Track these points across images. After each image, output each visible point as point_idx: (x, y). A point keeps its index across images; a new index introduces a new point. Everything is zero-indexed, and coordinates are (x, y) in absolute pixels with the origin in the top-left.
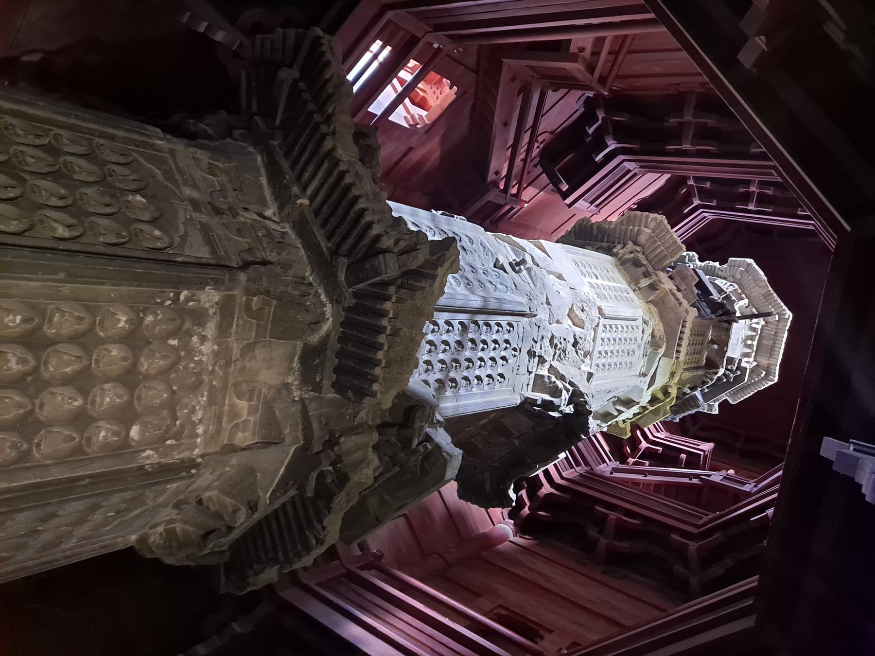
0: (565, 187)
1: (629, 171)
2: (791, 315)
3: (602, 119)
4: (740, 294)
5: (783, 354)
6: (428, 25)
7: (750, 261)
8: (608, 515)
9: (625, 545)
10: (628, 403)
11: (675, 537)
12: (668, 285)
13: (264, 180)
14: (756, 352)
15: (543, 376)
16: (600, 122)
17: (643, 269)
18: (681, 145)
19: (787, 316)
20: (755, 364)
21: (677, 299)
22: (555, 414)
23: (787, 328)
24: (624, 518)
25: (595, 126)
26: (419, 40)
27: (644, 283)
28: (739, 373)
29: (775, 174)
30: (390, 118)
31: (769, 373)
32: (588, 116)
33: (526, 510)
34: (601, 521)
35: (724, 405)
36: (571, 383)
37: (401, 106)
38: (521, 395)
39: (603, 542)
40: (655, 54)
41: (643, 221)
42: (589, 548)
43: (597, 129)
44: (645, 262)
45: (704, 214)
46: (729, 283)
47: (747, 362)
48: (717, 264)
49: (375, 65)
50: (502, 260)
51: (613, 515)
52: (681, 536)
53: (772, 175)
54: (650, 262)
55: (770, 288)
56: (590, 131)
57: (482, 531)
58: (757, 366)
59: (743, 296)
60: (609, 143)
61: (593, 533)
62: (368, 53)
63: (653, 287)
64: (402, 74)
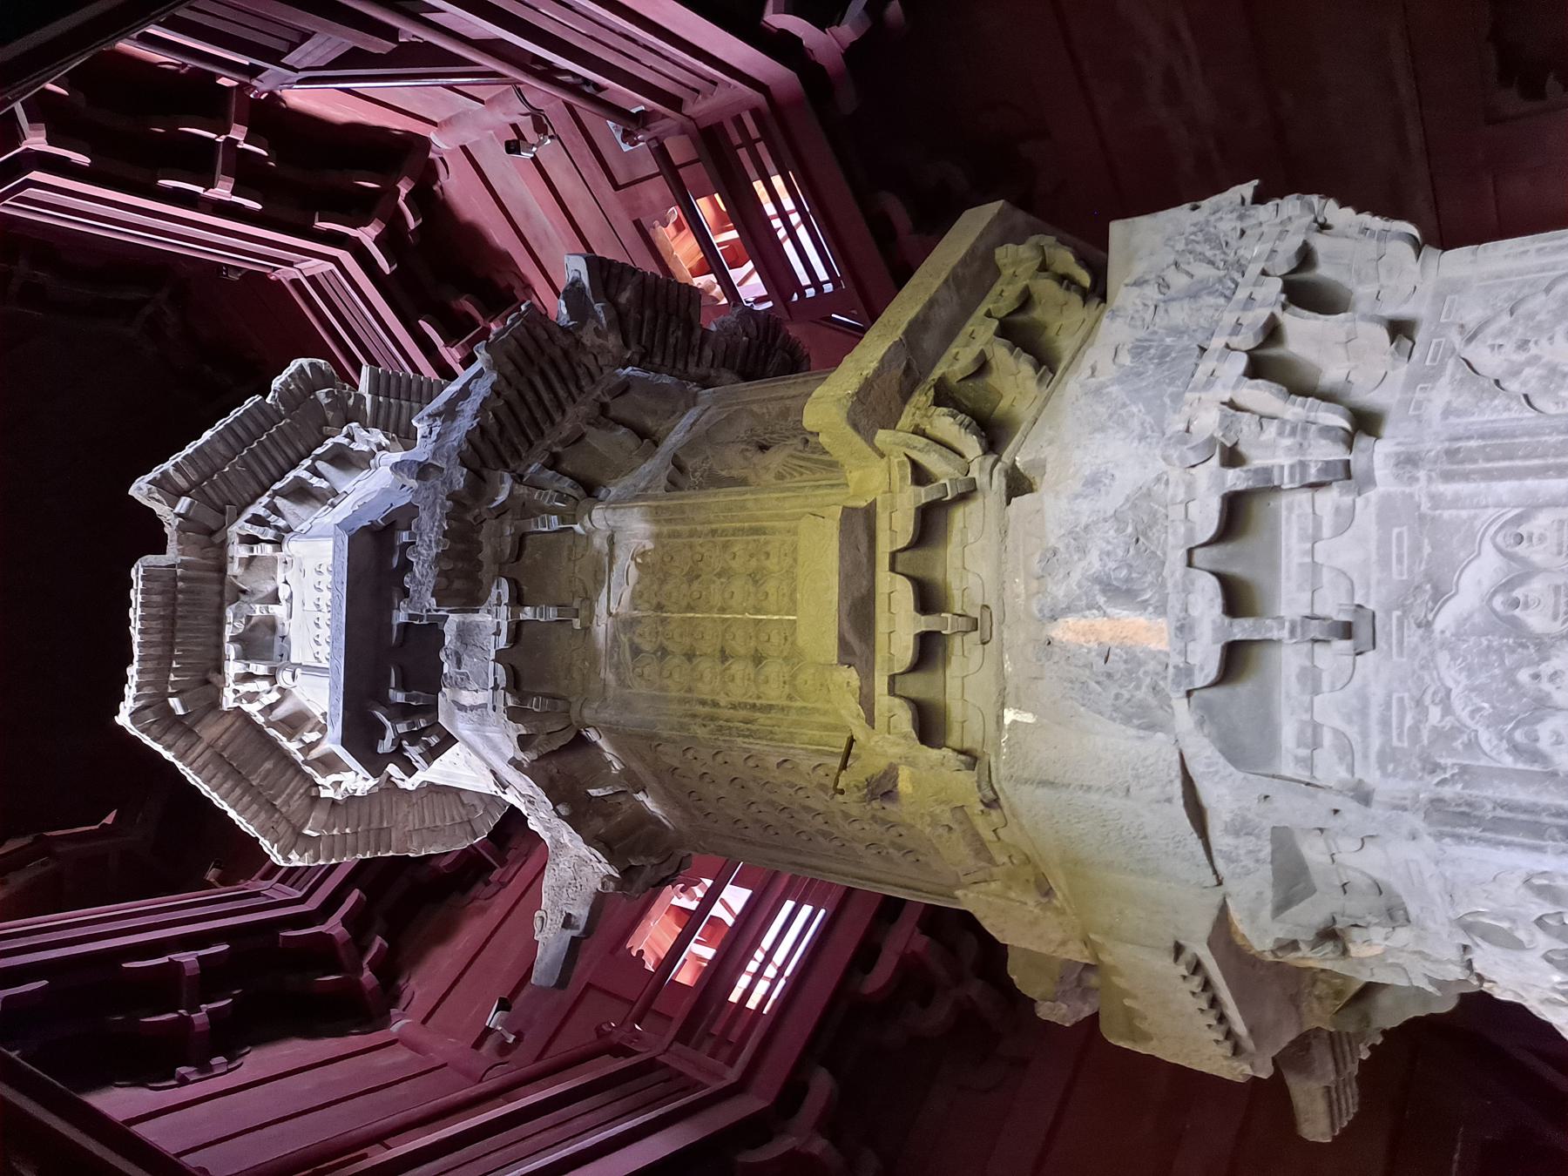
3: (362, 969)
5: (124, 680)
6: (666, 1066)
8: (233, 193)
11: (82, 159)
16: (365, 964)
24: (200, 190)
26: (676, 1038)
30: (748, 893)
32: (391, 971)
33: (404, 188)
34: (247, 174)
37: (737, 910)
40: (266, 1130)
49: (767, 943)
51: (222, 191)
62: (739, 151)
64: (708, 953)
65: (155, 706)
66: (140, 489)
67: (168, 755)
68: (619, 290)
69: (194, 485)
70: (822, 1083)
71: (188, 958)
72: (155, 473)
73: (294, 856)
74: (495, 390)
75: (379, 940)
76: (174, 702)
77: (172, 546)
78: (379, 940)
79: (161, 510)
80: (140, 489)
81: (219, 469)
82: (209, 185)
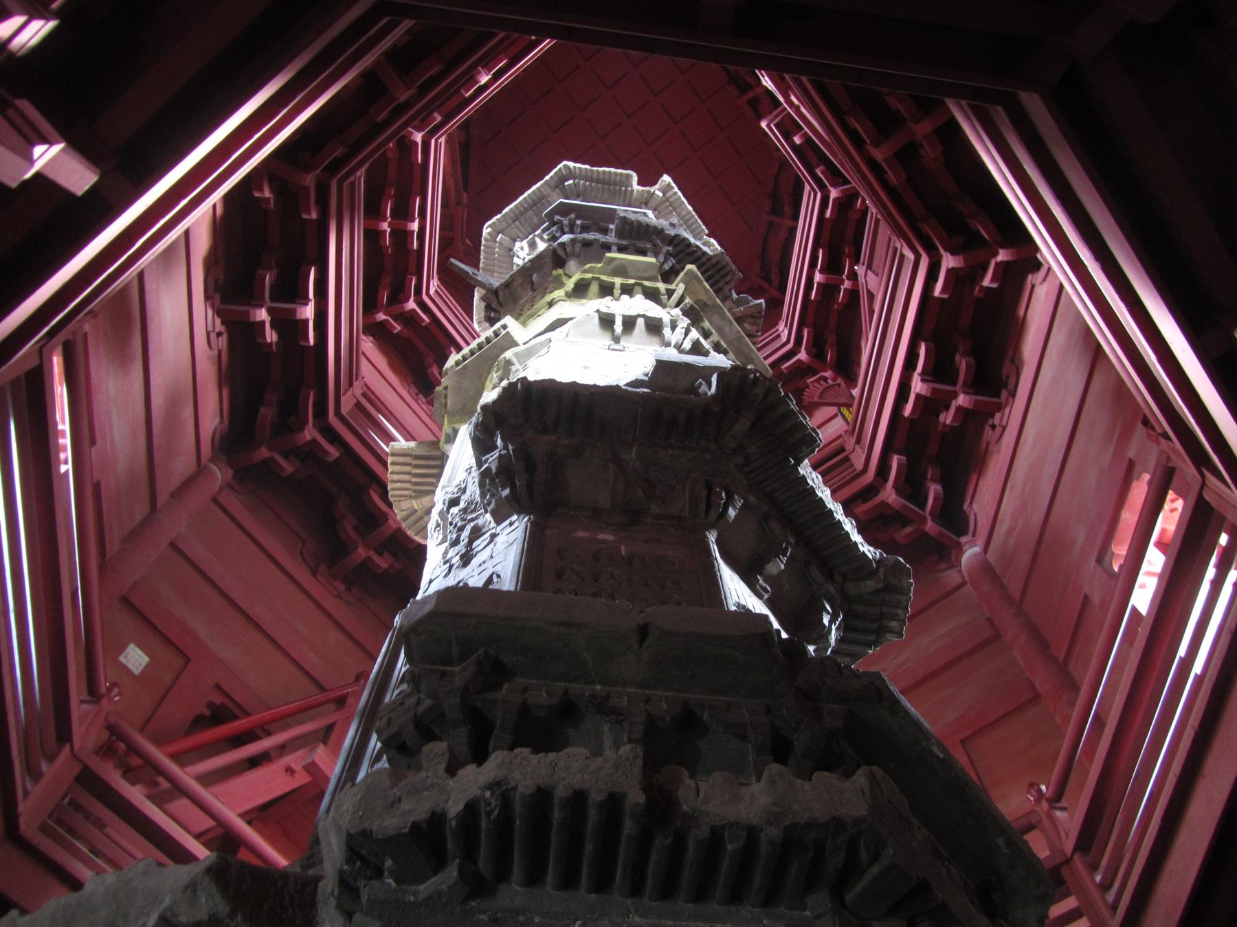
1: (358, 405)
9: (963, 364)
10: (607, 321)
11: (828, 214)
15: (493, 514)
18: (307, 321)
29: (352, 179)
35: (648, 179)
39: (962, 400)
42: (975, 422)
45: (432, 292)
52: (936, 281)
53: (353, 183)
57: (803, 821)
60: (309, 438)
61: (947, 418)
65: (571, 174)
66: (666, 178)
67: (547, 178)
68: (750, 324)
69: (667, 200)
70: (334, 452)
71: (415, 226)
72: (673, 184)
73: (489, 230)
74: (705, 253)
75: (399, 328)
76: (571, 182)
77: (641, 188)
78: (399, 328)
79: (657, 186)
80: (666, 178)
81: (674, 209)
82: (821, 272)
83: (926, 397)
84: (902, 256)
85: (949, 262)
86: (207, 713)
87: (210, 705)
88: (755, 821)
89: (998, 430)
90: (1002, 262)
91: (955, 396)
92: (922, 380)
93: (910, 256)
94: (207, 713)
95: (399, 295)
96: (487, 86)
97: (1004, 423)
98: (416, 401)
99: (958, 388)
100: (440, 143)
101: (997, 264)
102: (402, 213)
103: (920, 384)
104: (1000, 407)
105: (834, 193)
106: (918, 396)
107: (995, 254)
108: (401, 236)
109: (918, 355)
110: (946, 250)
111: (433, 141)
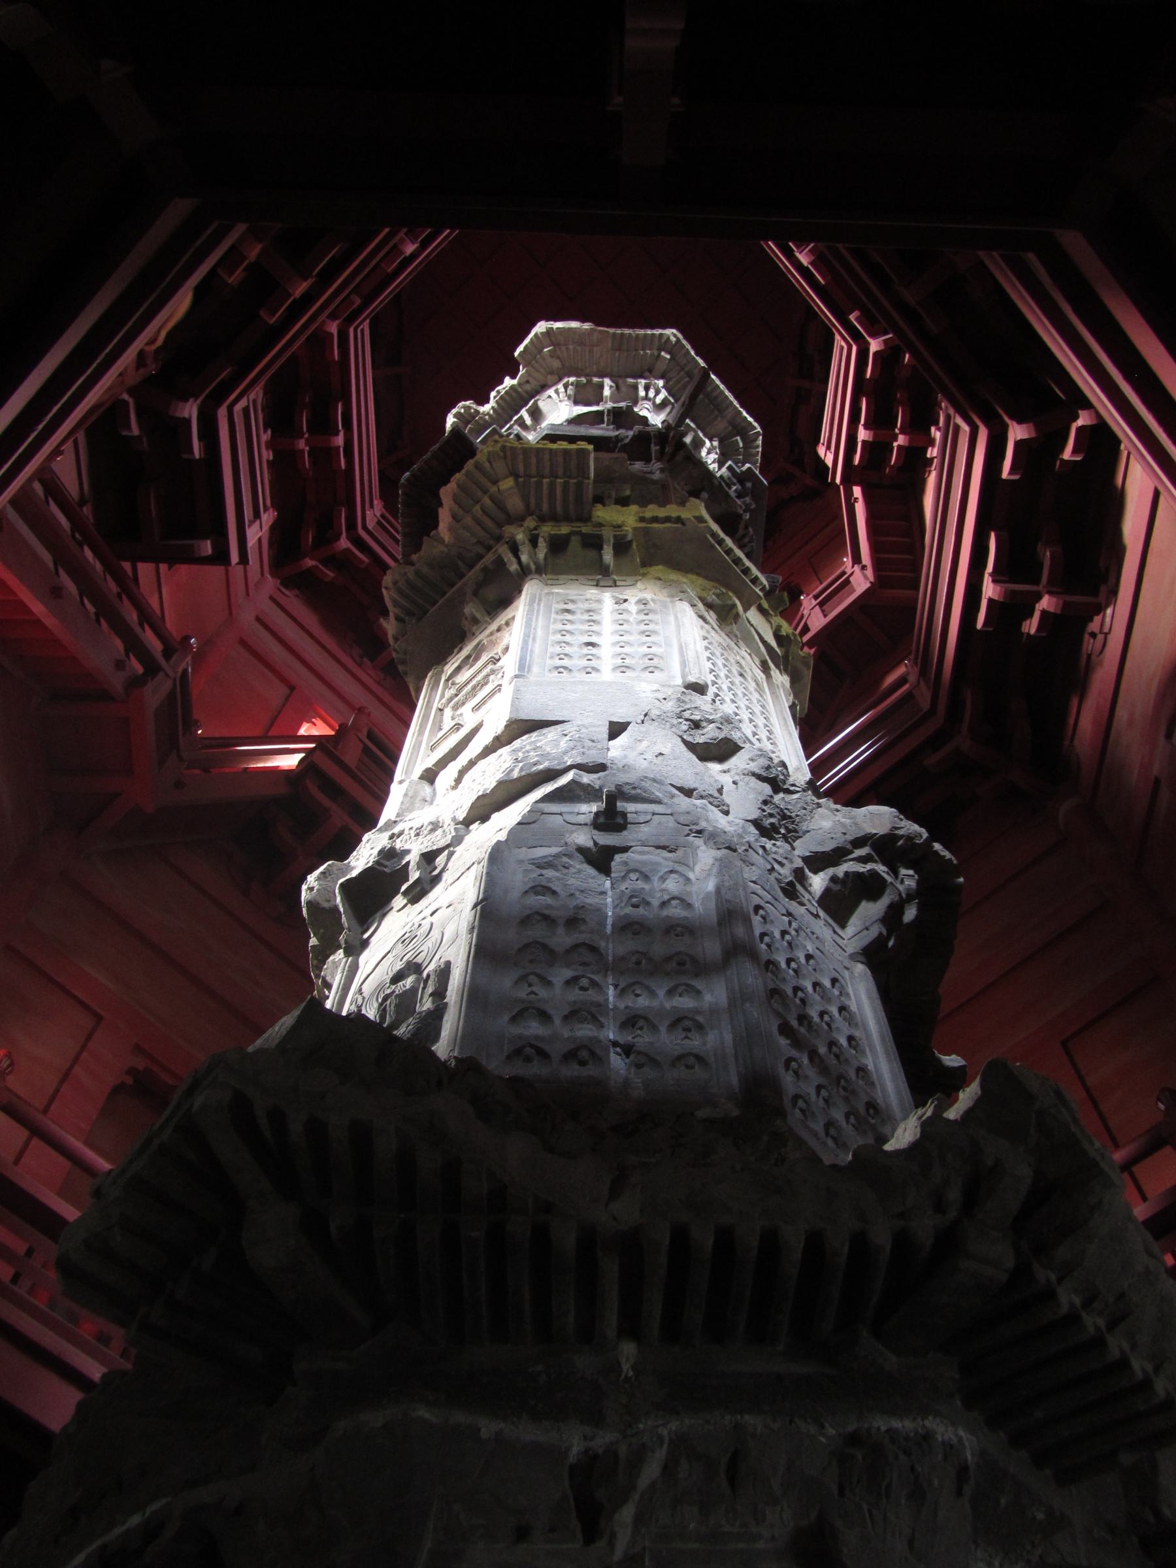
0: (207, 548)
2: (674, 331)
4: (589, 382)
7: (541, 327)
12: (628, 518)
13: (488, 1427)
14: (698, 427)
16: (131, 401)
17: (575, 542)
19: (673, 339)
20: (716, 443)
21: (668, 519)
22: (910, 914)
23: (693, 353)
25: (133, 416)
27: (608, 556)
28: (749, 485)
31: (742, 429)
36: (858, 842)
38: (852, 957)
39: (1046, 603)
41: (483, 480)
42: (1069, 629)
43: (139, 416)
44: (565, 530)
46: (560, 387)
47: (709, 453)
48: (508, 382)
50: (583, 838)
54: (567, 519)
55: (612, 330)
56: (136, 431)
58: (720, 442)
59: (596, 379)
60: (187, 416)
61: (1031, 626)
63: (622, 547)
71: (340, 440)
83: (1055, 615)
84: (957, 428)
85: (1017, 433)
86: (129, 1081)
87: (131, 1071)
88: (692, 499)
89: (1100, 637)
90: (1083, 426)
91: (1039, 598)
92: (993, 581)
93: (965, 428)
94: (129, 1081)
95: (326, 534)
96: (414, 256)
97: (1106, 630)
98: (360, 665)
99: (1040, 588)
100: (361, 333)
101: (1080, 430)
102: (323, 425)
103: (991, 585)
104: (1099, 609)
105: (875, 346)
106: (990, 600)
107: (1076, 418)
108: (323, 455)
109: (362, 552)
110: (1011, 418)
111: (351, 330)
